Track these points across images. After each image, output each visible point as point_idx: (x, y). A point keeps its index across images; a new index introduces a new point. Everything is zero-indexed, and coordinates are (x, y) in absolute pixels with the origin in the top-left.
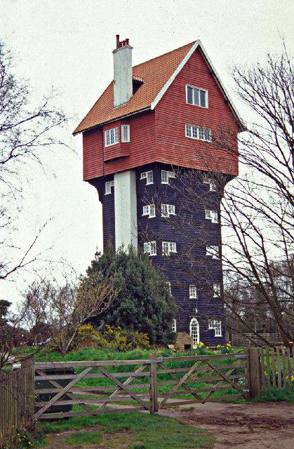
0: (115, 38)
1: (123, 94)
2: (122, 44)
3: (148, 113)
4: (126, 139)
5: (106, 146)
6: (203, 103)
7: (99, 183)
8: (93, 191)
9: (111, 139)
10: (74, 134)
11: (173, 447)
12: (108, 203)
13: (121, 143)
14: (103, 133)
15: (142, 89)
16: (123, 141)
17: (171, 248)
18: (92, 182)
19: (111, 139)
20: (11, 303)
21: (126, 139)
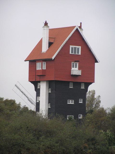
0: (15, 87)
1: (45, 48)
2: (46, 24)
3: (51, 60)
4: (44, 68)
5: (37, 69)
6: (78, 53)
7: (36, 83)
8: (32, 86)
9: (39, 67)
10: (25, 61)
11: (40, 153)
12: (38, 91)
13: (42, 70)
14: (36, 64)
15: (52, 46)
16: (43, 69)
17: (71, 102)
18: (32, 82)
19: (39, 67)
20: (46, 21)
21: (44, 68)
